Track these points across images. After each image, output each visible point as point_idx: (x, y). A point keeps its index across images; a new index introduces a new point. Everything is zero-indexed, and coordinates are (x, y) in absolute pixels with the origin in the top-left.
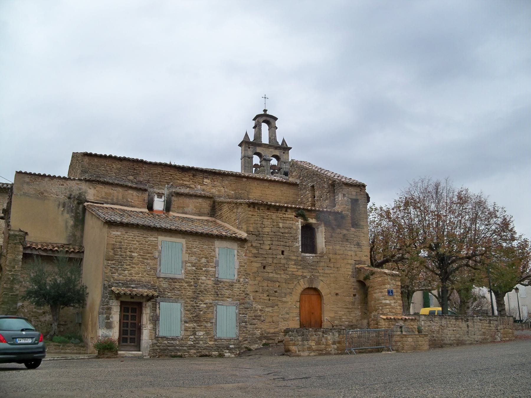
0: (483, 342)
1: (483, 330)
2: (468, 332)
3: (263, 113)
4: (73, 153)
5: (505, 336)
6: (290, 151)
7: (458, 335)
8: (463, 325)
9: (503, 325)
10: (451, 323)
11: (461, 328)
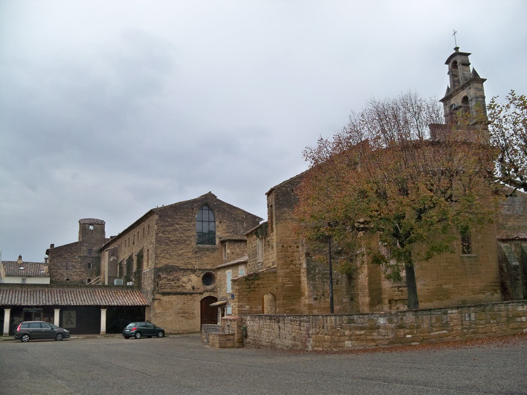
0: (292, 351)
1: (293, 334)
2: (279, 335)
3: (454, 51)
4: (210, 192)
5: (317, 344)
6: (484, 84)
7: (271, 338)
8: (276, 326)
9: (315, 328)
10: (266, 324)
11: (273, 330)
